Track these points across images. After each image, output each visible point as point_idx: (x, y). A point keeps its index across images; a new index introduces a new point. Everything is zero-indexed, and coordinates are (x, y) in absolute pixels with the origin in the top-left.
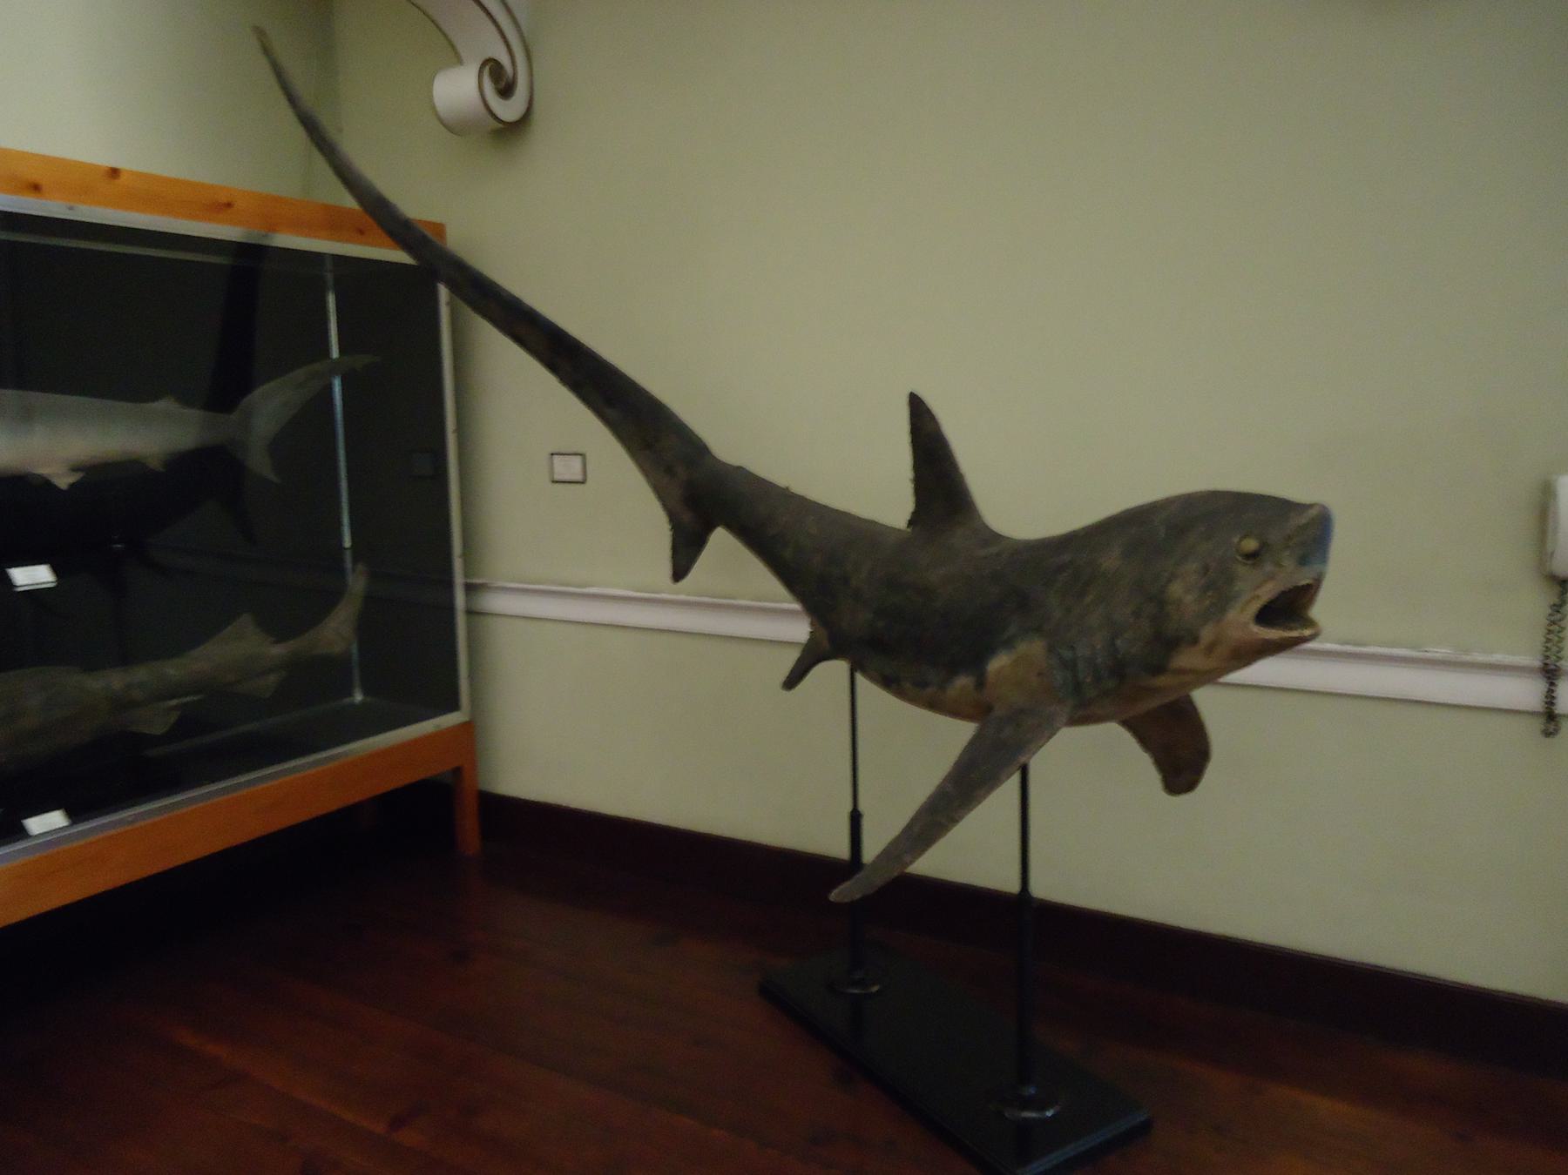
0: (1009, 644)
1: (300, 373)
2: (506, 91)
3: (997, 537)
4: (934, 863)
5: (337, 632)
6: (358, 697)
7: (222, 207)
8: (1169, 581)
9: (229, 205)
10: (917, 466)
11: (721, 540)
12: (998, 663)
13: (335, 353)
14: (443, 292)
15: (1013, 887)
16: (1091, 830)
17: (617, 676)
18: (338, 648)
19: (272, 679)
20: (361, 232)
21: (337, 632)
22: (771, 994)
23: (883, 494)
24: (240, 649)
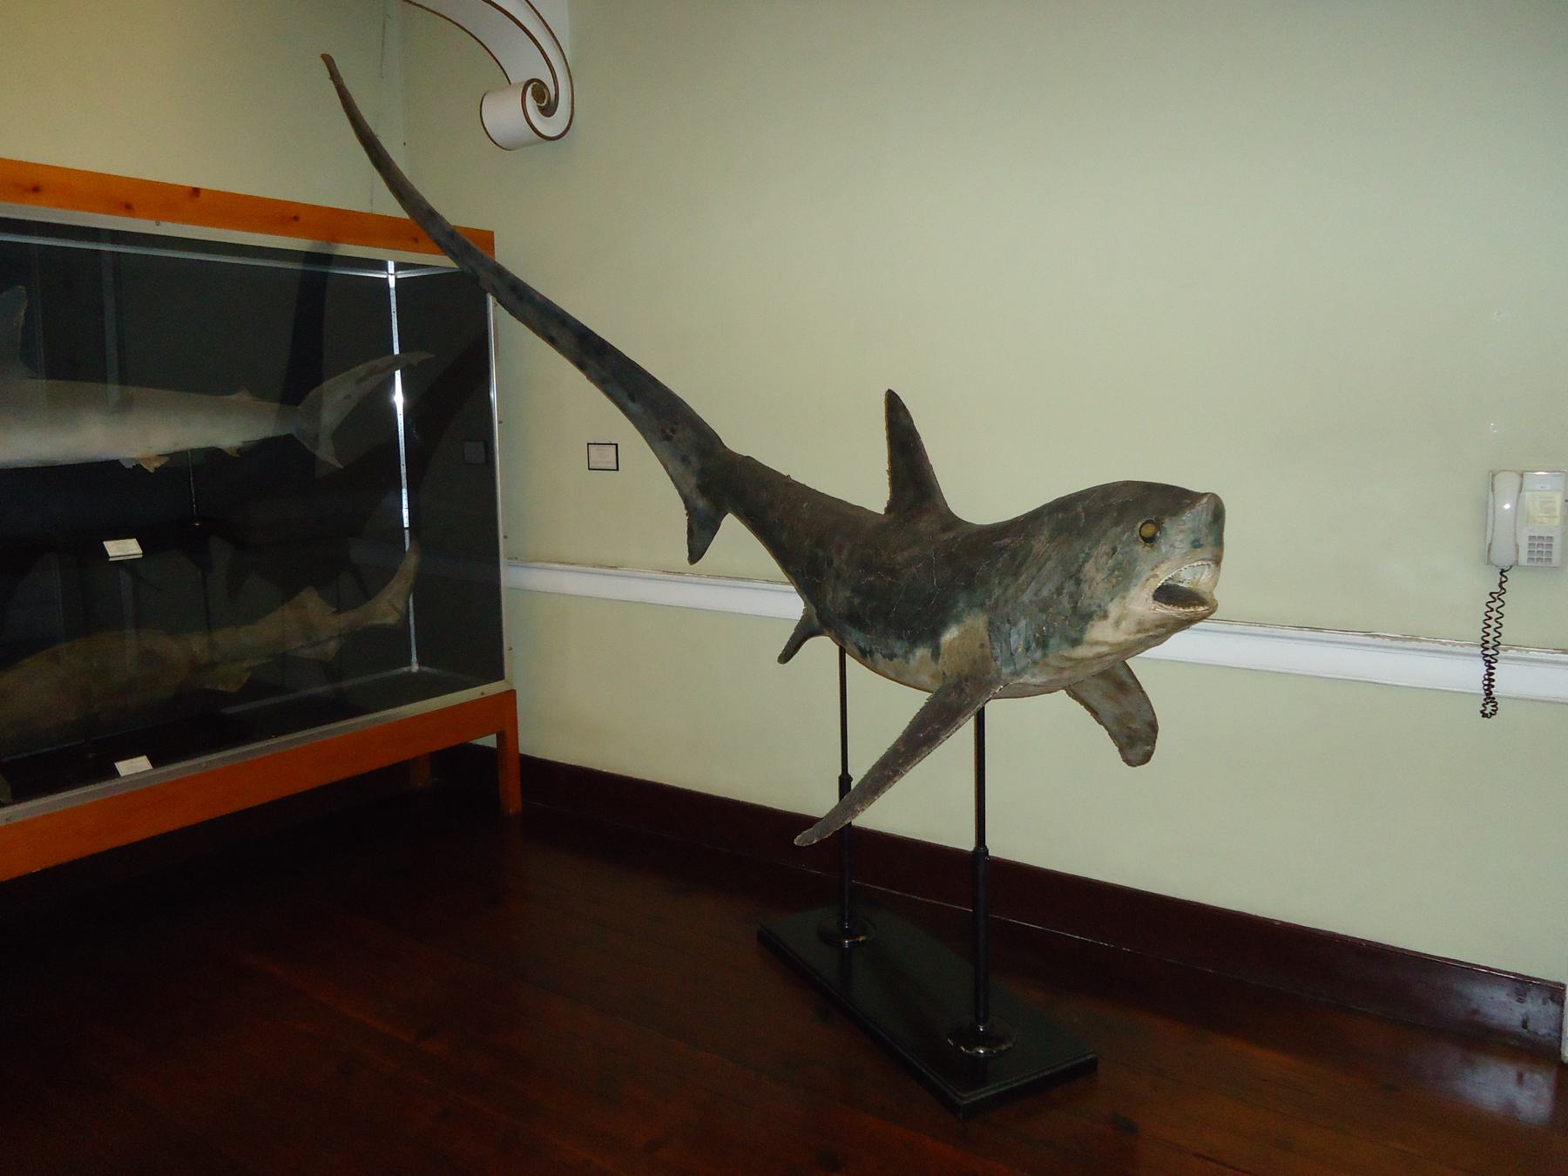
0: (958, 620)
1: (361, 370)
2: (548, 110)
3: (958, 522)
4: (888, 815)
5: (392, 605)
6: (415, 668)
7: (285, 216)
8: (1085, 561)
9: (296, 218)
10: (893, 460)
11: (732, 527)
12: (950, 635)
13: (396, 352)
14: (491, 299)
15: (969, 845)
16: (1040, 791)
17: (659, 659)
18: (392, 619)
19: (332, 646)
20: (416, 240)
21: (392, 605)
22: (770, 944)
23: (866, 486)
24: (308, 624)
